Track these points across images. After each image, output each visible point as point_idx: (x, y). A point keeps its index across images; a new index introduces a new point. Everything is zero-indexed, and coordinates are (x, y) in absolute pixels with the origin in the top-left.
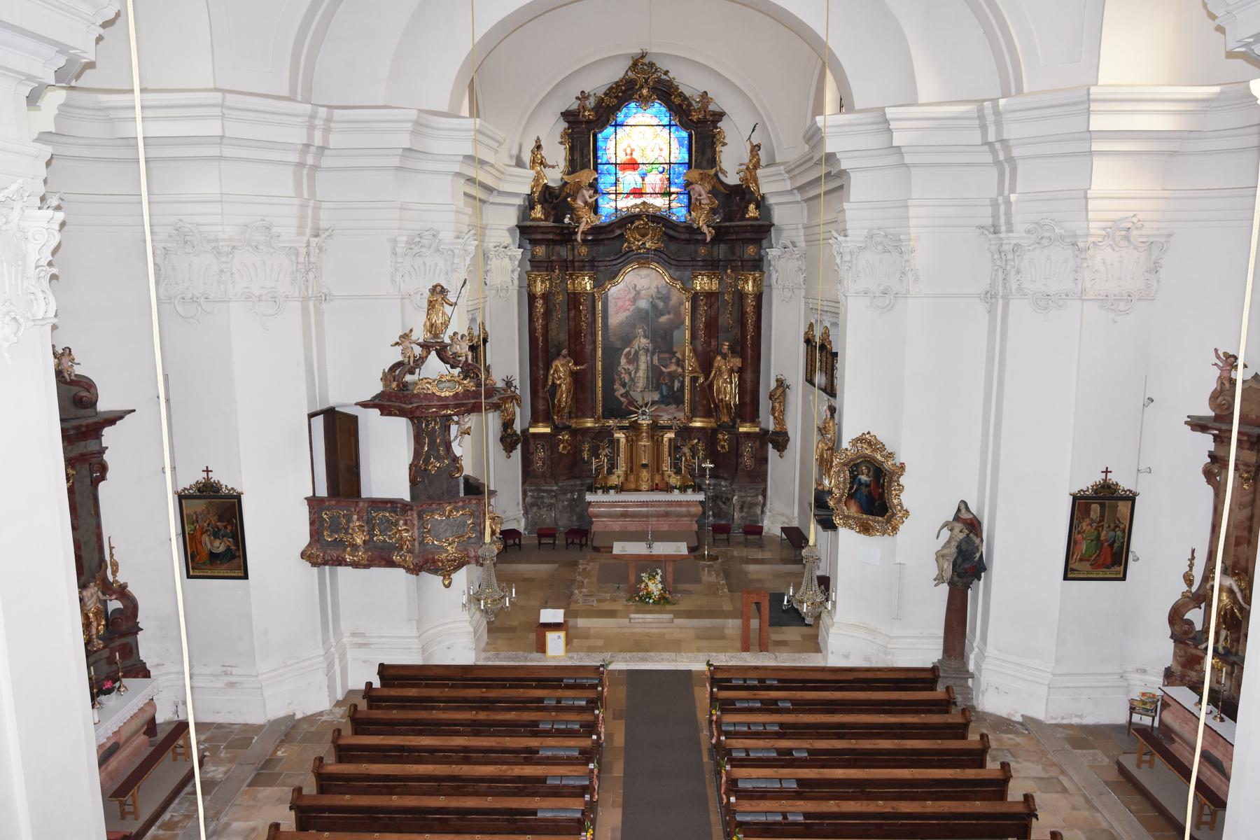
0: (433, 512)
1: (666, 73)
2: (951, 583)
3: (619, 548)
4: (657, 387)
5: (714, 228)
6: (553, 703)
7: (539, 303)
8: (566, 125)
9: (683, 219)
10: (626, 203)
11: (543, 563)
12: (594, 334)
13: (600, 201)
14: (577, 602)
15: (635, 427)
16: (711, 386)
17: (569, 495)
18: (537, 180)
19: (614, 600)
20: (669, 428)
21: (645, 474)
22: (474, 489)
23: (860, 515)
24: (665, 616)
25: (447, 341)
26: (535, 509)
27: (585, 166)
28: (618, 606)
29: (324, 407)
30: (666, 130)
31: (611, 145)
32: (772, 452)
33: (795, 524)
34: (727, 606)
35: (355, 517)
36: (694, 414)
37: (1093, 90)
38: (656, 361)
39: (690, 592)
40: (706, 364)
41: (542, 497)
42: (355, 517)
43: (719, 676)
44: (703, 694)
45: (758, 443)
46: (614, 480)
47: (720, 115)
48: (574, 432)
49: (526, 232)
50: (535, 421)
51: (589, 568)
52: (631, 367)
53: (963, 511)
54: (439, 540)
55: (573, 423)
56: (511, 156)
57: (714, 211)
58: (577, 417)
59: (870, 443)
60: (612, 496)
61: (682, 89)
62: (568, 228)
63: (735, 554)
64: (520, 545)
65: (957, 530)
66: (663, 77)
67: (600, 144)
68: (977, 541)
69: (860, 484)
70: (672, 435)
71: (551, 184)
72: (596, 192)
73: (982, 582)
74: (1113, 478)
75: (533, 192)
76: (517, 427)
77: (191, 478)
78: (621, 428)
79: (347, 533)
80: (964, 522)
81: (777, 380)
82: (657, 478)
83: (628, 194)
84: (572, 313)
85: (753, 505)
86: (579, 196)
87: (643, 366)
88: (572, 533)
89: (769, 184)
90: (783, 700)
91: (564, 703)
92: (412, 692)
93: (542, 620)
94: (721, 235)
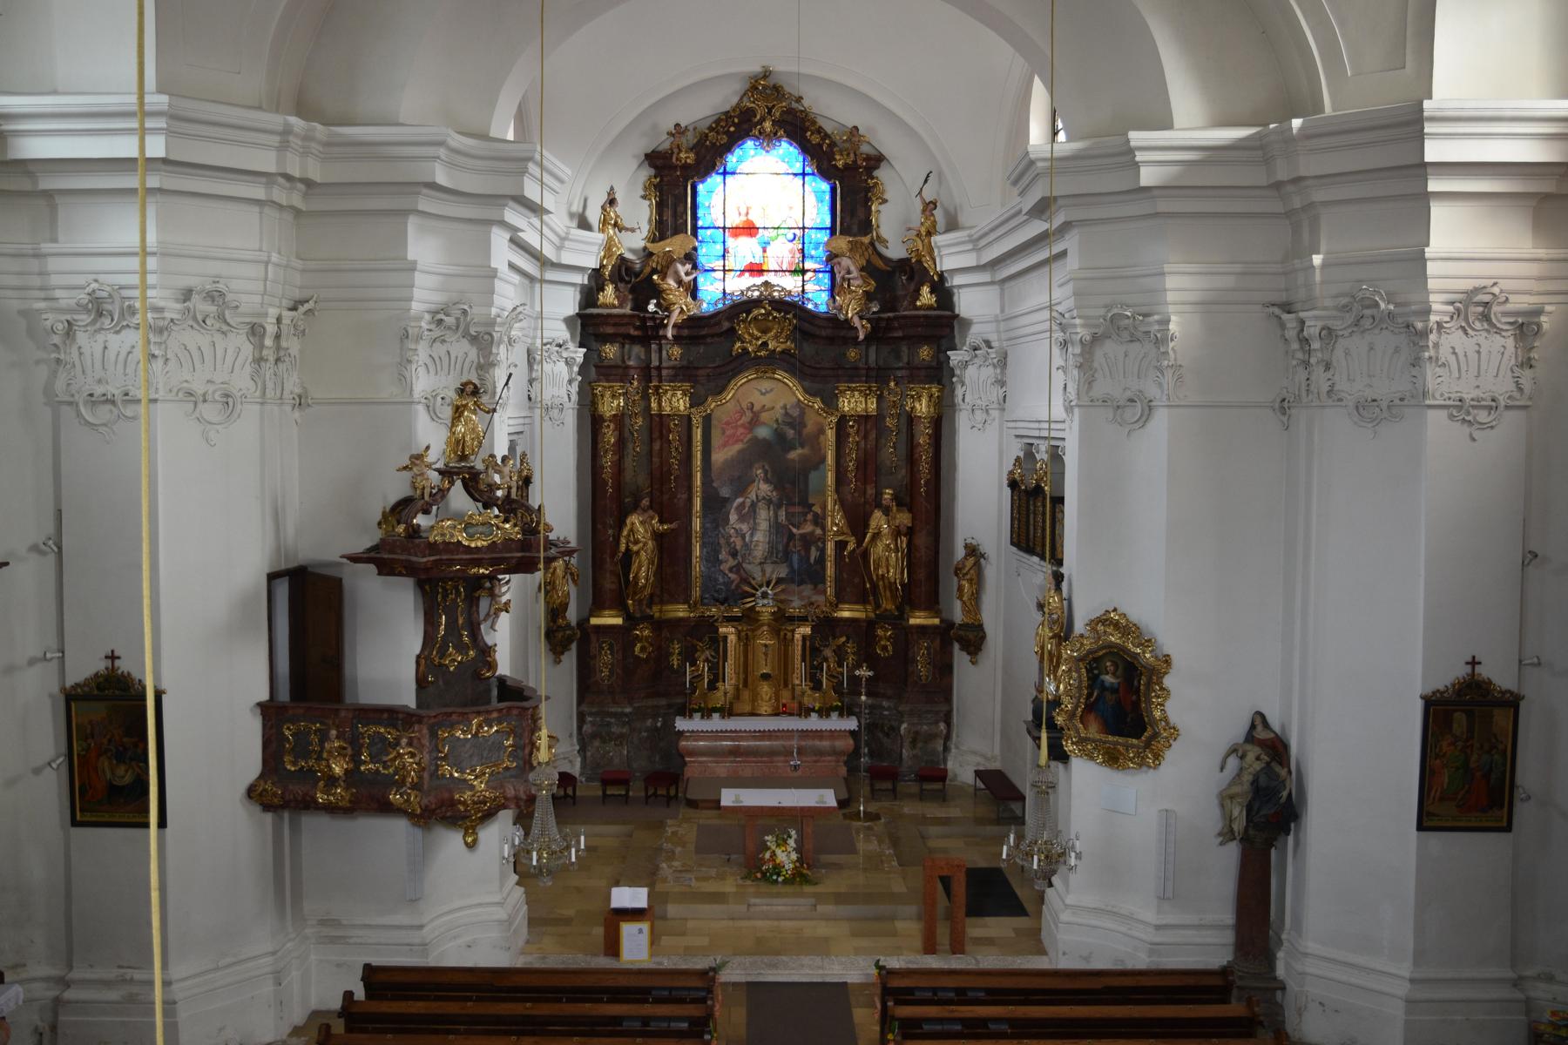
0: (452, 726)
1: (799, 99)
2: (1246, 840)
3: (728, 797)
4: (786, 557)
5: (869, 320)
6: (637, 1025)
7: (609, 436)
8: (652, 172)
9: (823, 308)
10: (739, 285)
11: (607, 823)
12: (689, 477)
13: (701, 280)
14: (665, 880)
15: (750, 617)
16: (865, 555)
17: (649, 722)
18: (608, 247)
19: (721, 877)
20: (803, 620)
21: (765, 689)
22: (512, 693)
23: (1103, 737)
24: (802, 901)
25: (480, 466)
26: (597, 743)
27: (679, 229)
28: (729, 886)
29: (292, 565)
30: (799, 180)
31: (717, 200)
32: (960, 658)
33: (995, 765)
34: (898, 886)
35: (334, 732)
36: (840, 598)
37: (1427, 104)
38: (782, 515)
39: (838, 867)
40: (858, 523)
41: (609, 724)
42: (334, 732)
43: (896, 983)
44: (866, 1018)
45: (938, 641)
46: (718, 698)
47: (877, 160)
48: (659, 625)
49: (590, 325)
50: (598, 606)
51: (681, 831)
52: (744, 527)
53: (1259, 728)
54: (462, 772)
55: (655, 611)
56: (571, 215)
57: (868, 296)
58: (662, 602)
59: (1116, 625)
60: (716, 723)
61: (821, 122)
62: (653, 319)
63: (906, 810)
64: (574, 797)
65: (1251, 757)
66: (794, 105)
67: (700, 199)
68: (1283, 772)
69: (1103, 688)
70: (807, 630)
71: (629, 256)
72: (695, 267)
73: (1291, 839)
74: (1484, 671)
75: (602, 266)
76: (572, 615)
77: (84, 666)
78: (730, 620)
79: (319, 758)
80: (1262, 744)
81: (966, 546)
82: (785, 696)
83: (743, 272)
84: (657, 446)
85: (932, 737)
86: (670, 272)
87: (764, 526)
88: (653, 779)
89: (950, 256)
90: (997, 1020)
91: (653, 1026)
92: (418, 1007)
93: (615, 904)
94: (879, 333)
